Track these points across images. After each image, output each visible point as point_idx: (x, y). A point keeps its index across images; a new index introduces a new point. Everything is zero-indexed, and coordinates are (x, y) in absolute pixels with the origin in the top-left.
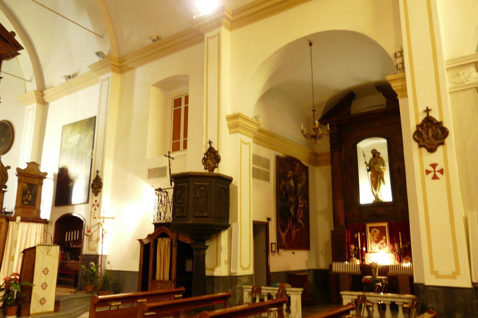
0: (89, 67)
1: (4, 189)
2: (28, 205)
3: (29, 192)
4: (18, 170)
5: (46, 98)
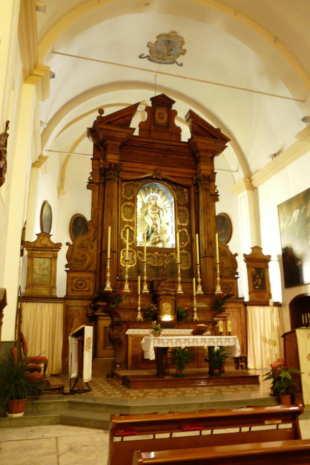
0: (296, 137)
1: (236, 276)
2: (259, 289)
3: (258, 276)
4: (245, 255)
5: (255, 183)
